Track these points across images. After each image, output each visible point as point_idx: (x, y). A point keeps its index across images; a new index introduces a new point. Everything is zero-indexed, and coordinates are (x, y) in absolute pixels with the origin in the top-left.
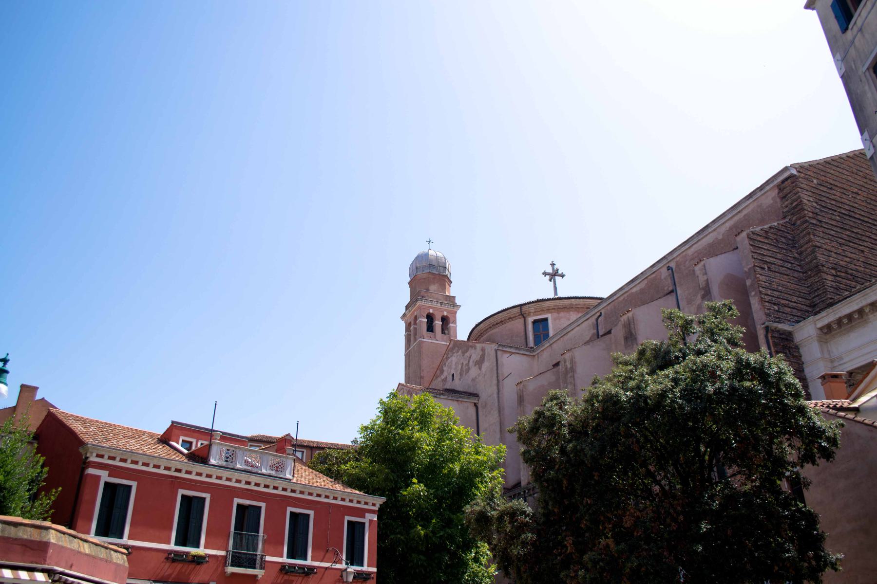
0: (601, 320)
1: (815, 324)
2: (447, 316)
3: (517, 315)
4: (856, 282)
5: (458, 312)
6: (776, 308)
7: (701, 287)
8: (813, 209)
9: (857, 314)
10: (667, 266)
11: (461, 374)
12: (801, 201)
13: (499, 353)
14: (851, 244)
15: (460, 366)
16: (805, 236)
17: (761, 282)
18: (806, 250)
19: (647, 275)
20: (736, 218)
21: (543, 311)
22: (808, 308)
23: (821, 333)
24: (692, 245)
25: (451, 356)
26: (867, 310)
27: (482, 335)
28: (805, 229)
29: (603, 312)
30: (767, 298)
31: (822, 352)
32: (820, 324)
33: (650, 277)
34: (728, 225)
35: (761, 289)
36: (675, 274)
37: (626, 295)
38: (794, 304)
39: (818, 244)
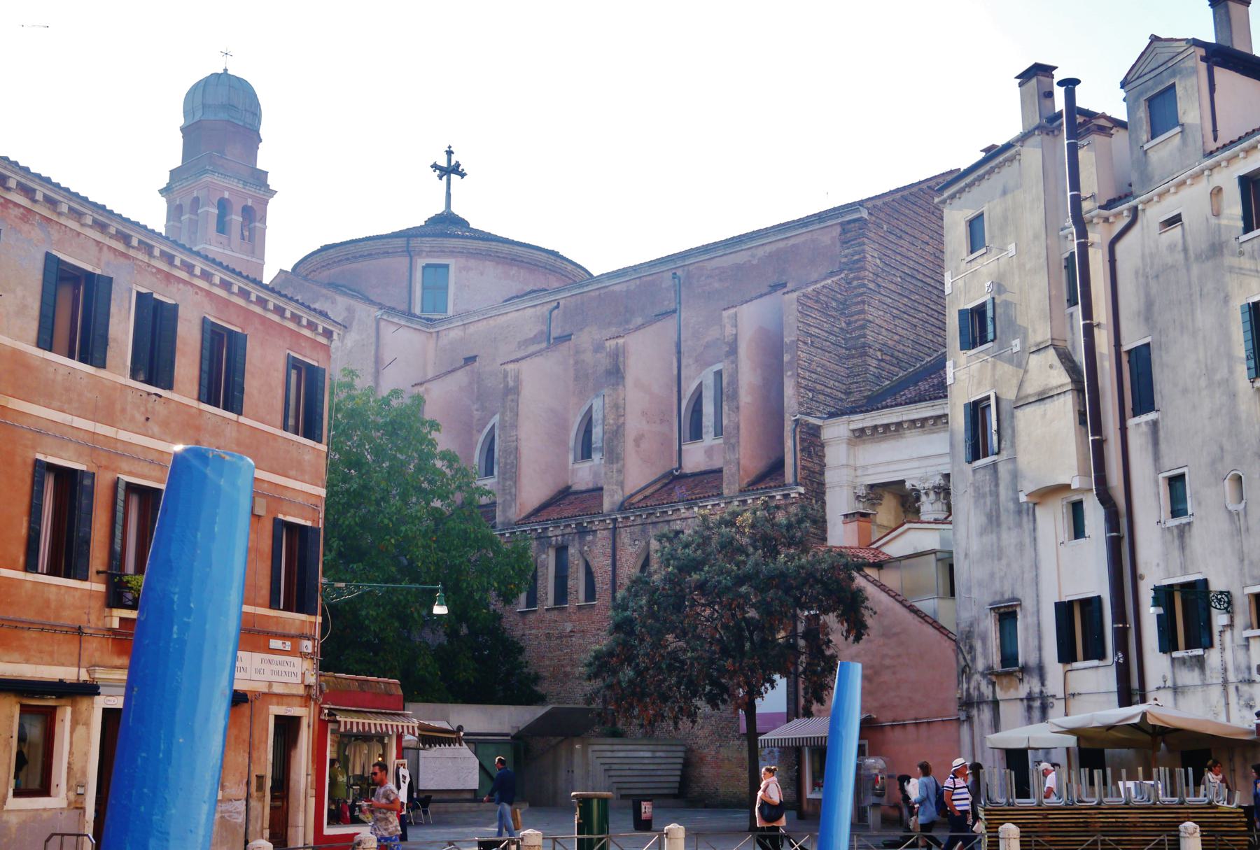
2: (251, 207)
4: (900, 368)
5: (271, 201)
6: (810, 395)
8: (875, 268)
9: (894, 426)
10: (674, 271)
12: (865, 257)
13: (382, 324)
14: (906, 316)
16: (858, 303)
17: (801, 362)
18: (855, 322)
20: (781, 245)
21: (443, 252)
22: (840, 395)
26: (905, 426)
27: (329, 267)
28: (862, 294)
29: (562, 302)
30: (804, 382)
31: (848, 456)
32: (853, 426)
33: (645, 279)
34: (768, 249)
35: (800, 371)
36: (683, 289)
37: (602, 291)
38: (829, 390)
39: (870, 318)
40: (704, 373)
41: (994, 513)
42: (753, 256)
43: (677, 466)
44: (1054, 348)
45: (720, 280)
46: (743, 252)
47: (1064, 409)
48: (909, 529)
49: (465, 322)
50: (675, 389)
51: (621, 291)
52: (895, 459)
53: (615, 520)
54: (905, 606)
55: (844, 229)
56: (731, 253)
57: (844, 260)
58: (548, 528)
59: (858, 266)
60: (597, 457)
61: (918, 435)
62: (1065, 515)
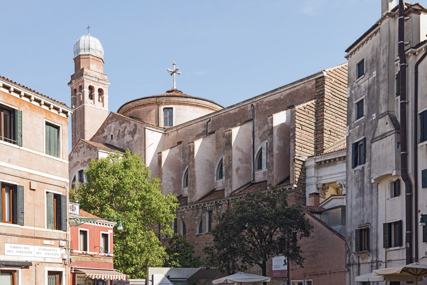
0: (210, 124)
1: (315, 160)
3: (154, 102)
7: (269, 129)
10: (252, 104)
11: (118, 137)
15: (117, 132)
18: (320, 119)
19: (240, 106)
20: (292, 90)
23: (317, 165)
24: (267, 97)
25: (111, 123)
26: (337, 160)
29: (211, 119)
31: (315, 173)
32: (317, 161)
33: (241, 107)
34: (287, 92)
36: (255, 110)
37: (226, 113)
40: (263, 143)
41: (362, 188)
42: (281, 95)
43: (253, 180)
44: (389, 115)
45: (269, 106)
46: (278, 94)
47: (392, 140)
48: (333, 198)
49: (177, 129)
50: (252, 150)
51: (233, 113)
52: (333, 173)
53: (228, 200)
54: (327, 227)
55: (317, 81)
56: (273, 95)
57: (316, 94)
58: (205, 204)
59: (322, 96)
60: (224, 178)
61: (342, 163)
62: (390, 187)
